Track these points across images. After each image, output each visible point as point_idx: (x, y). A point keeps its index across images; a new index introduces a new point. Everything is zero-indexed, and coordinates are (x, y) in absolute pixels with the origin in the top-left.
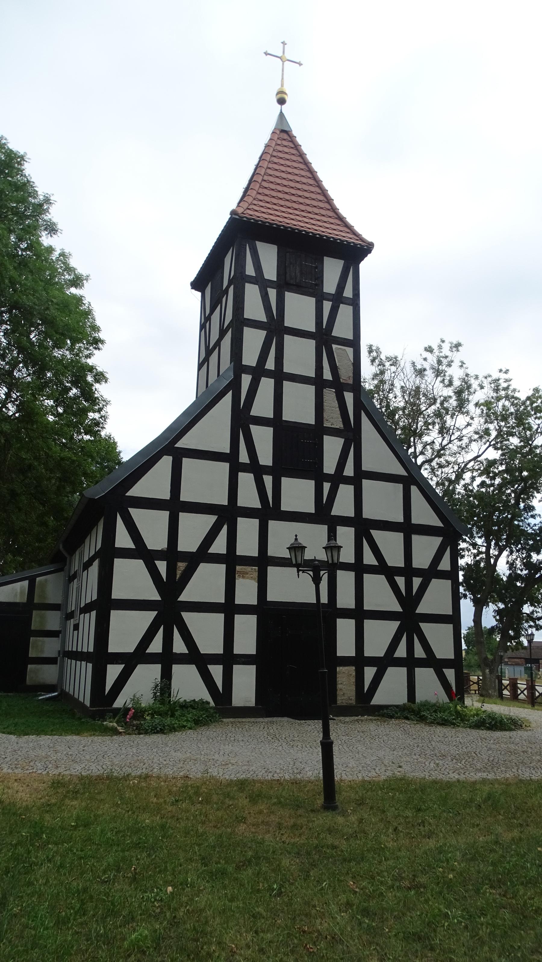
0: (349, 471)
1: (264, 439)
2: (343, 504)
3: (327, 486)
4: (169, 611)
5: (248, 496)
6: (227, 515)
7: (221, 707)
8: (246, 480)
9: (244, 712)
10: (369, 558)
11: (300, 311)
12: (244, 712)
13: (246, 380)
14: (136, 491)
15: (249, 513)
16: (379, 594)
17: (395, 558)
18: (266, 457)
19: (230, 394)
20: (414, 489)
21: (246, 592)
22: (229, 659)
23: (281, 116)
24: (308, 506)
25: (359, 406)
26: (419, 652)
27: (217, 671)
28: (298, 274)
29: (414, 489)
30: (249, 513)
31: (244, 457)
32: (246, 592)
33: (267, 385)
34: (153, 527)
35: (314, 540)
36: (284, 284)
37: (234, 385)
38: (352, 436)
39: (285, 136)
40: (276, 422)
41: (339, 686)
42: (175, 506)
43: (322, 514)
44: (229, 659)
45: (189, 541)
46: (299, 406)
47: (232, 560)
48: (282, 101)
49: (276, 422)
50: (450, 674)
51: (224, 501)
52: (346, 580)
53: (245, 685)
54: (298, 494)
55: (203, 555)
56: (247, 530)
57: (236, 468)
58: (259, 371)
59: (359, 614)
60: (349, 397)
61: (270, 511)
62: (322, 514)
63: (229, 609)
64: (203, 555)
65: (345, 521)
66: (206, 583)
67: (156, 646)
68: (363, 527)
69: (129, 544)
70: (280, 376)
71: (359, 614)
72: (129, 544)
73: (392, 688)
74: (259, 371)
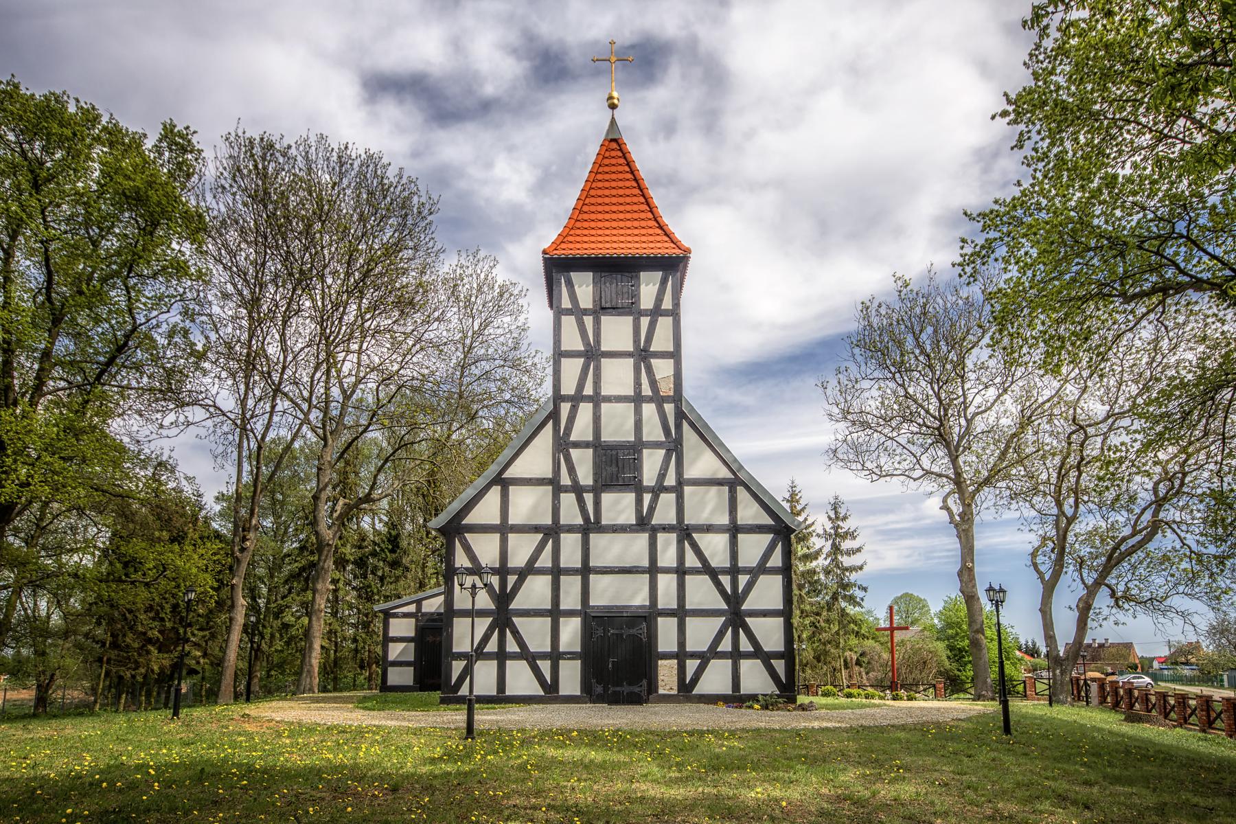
0: (670, 480)
1: (584, 461)
2: (665, 512)
3: (647, 498)
4: (503, 618)
5: (570, 512)
6: (552, 532)
7: (551, 692)
8: (568, 499)
9: (667, 699)
10: (691, 560)
11: (617, 332)
12: (667, 699)
13: (565, 408)
14: (470, 519)
15: (571, 529)
16: (701, 592)
17: (719, 559)
18: (585, 476)
19: (550, 424)
20: (742, 493)
21: (571, 598)
22: (555, 656)
23: (613, 122)
24: (629, 517)
25: (680, 415)
26: (745, 645)
27: (545, 666)
28: (614, 296)
29: (742, 493)
30: (571, 529)
31: (565, 480)
32: (571, 598)
33: (585, 410)
34: (486, 549)
35: (634, 548)
36: (601, 309)
37: (554, 415)
38: (674, 447)
39: (614, 145)
40: (597, 445)
41: (660, 678)
42: (504, 529)
43: (643, 523)
44: (555, 656)
45: (518, 559)
46: (618, 425)
47: (556, 572)
48: (613, 107)
49: (597, 445)
50: (779, 665)
51: (548, 521)
52: (667, 584)
53: (571, 677)
54: (619, 507)
55: (530, 569)
56: (570, 546)
57: (558, 489)
58: (577, 399)
59: (681, 613)
60: (669, 408)
61: (590, 526)
62: (643, 523)
63: (555, 613)
64: (530, 569)
65: (666, 529)
66: (536, 591)
67: (492, 646)
68: (685, 533)
69: (468, 564)
70: (597, 400)
71: (681, 613)
72: (468, 564)
73: (716, 679)
74: (577, 399)
